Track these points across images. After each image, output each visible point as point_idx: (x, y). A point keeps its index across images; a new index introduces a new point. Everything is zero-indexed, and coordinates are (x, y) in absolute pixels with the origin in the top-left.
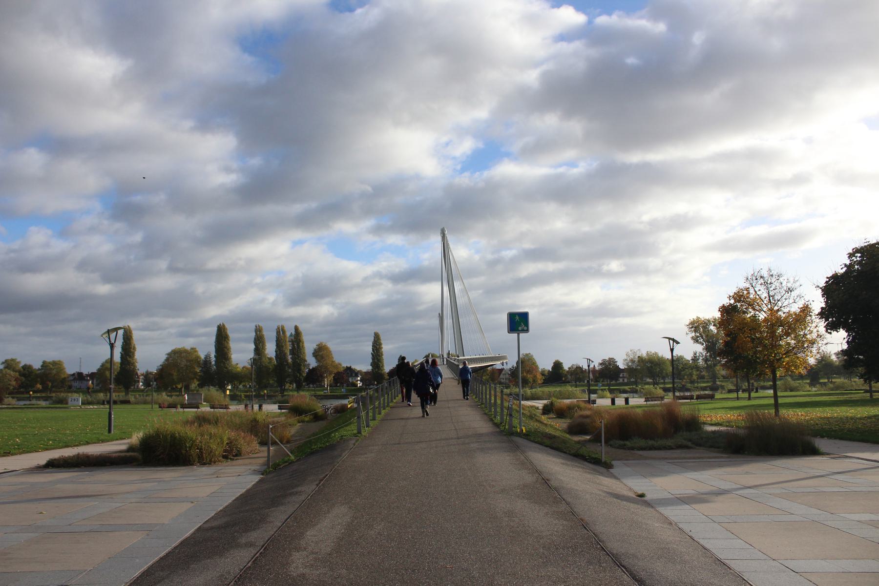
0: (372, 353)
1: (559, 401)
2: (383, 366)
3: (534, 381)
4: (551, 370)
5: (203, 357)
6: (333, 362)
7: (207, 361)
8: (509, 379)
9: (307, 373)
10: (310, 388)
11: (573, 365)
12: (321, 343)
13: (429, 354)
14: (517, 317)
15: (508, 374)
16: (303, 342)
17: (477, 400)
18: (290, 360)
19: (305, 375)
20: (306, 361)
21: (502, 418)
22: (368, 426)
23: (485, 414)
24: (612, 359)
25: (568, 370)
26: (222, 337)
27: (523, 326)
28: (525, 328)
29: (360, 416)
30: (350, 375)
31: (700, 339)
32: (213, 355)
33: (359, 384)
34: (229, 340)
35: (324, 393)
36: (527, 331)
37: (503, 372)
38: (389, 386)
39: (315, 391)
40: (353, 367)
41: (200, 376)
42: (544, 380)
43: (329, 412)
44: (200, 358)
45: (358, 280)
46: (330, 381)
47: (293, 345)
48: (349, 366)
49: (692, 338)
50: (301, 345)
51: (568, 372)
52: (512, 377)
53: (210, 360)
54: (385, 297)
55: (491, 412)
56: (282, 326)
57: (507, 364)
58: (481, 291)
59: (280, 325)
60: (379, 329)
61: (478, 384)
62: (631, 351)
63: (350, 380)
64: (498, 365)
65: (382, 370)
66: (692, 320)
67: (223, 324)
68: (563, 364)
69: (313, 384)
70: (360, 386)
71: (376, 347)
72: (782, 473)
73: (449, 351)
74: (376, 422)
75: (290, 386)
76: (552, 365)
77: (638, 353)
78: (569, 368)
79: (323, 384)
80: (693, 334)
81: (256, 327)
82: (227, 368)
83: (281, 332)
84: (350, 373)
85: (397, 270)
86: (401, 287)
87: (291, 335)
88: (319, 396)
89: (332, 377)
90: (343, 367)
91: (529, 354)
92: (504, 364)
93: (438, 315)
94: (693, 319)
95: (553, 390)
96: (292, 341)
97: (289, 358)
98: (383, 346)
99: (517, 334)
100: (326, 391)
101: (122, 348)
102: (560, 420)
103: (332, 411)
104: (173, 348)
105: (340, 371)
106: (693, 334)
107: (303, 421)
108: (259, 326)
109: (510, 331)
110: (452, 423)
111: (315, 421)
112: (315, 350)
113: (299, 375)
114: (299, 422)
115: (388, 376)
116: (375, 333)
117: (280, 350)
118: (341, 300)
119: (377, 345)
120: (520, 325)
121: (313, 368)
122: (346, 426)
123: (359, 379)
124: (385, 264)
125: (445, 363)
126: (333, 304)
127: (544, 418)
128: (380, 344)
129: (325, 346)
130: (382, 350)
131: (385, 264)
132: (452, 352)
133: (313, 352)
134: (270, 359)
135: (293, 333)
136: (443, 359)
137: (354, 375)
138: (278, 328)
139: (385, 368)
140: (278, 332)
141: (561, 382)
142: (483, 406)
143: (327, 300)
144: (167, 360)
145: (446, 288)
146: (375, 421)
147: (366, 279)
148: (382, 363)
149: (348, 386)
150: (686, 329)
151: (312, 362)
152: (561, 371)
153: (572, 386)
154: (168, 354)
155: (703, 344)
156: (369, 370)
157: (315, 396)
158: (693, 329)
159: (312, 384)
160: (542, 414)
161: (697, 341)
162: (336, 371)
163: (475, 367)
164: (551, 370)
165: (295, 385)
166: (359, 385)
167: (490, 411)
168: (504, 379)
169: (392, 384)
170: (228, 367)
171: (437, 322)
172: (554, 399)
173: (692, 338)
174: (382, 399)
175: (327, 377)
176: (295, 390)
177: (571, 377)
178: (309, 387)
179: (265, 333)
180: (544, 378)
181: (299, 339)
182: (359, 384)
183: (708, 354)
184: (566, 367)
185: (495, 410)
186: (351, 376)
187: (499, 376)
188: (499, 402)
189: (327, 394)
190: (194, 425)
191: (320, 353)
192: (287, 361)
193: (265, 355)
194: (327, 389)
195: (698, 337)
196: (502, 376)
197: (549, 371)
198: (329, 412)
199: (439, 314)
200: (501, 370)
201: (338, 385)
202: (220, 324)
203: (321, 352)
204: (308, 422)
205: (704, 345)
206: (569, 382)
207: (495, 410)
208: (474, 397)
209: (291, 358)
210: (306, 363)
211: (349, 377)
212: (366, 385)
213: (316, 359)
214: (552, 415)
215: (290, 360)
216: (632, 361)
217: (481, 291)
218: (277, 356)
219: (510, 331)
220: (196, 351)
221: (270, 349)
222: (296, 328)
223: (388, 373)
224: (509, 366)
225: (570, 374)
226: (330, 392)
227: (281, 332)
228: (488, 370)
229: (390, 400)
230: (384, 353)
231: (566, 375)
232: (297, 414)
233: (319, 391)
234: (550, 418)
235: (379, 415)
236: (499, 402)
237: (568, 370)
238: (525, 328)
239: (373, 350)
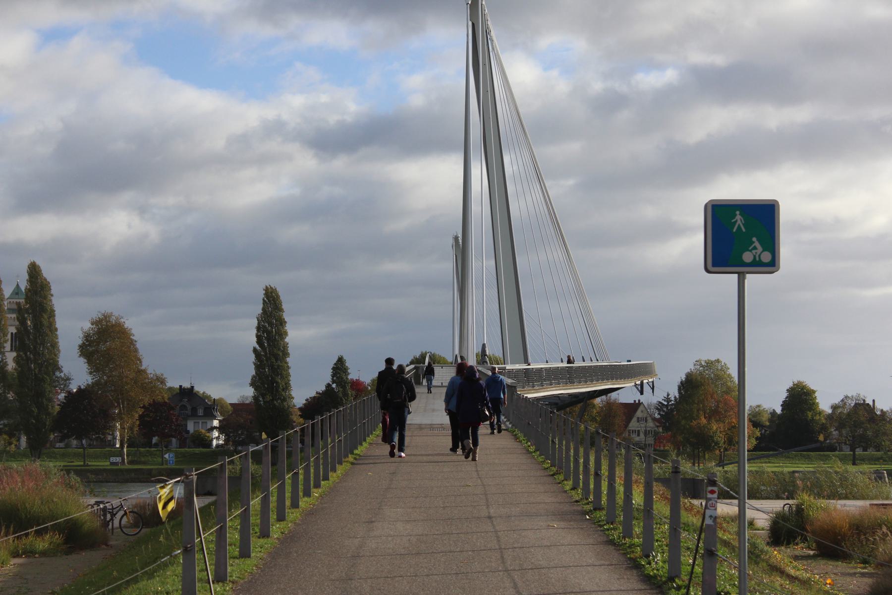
0: (255, 350)
1: (823, 503)
2: (287, 386)
3: (730, 441)
4: (779, 410)
8: (656, 434)
9: (64, 406)
10: (70, 450)
11: (846, 397)
12: (106, 317)
13: (426, 354)
14: (739, 218)
15: (654, 419)
17: (577, 495)
18: (11, 365)
19: (57, 408)
20: (60, 369)
21: (674, 561)
22: (220, 578)
23: (611, 542)
25: (830, 411)
27: (757, 250)
28: (766, 257)
29: (193, 546)
30: (189, 412)
33: (217, 439)
35: (112, 464)
36: (772, 265)
37: (639, 414)
39: (84, 457)
40: (200, 389)
42: (757, 439)
43: (116, 522)
45: (218, 143)
46: (131, 429)
47: (22, 321)
48: (186, 385)
51: (830, 417)
52: (666, 429)
54: (296, 191)
55: (631, 536)
57: (653, 389)
58: (571, 182)
60: (276, 281)
61: (581, 450)
63: (191, 427)
64: (626, 392)
65: (284, 400)
68: (816, 394)
69: (79, 438)
70: (218, 446)
71: (269, 333)
73: (484, 345)
74: (249, 565)
75: (10, 444)
76: (784, 395)
78: (835, 407)
79: (110, 438)
84: (189, 407)
85: (333, 119)
86: (340, 164)
87: (17, 292)
88: (98, 472)
89: (137, 416)
90: (170, 389)
91: (718, 361)
92: (647, 388)
93: (451, 241)
95: (786, 470)
96: (19, 310)
98: (288, 328)
99: (736, 276)
100: (119, 459)
102: (831, 566)
103: (125, 519)
105: (159, 399)
107: (29, 553)
109: (714, 265)
110: (506, 570)
111: (68, 552)
112: (87, 337)
113: (35, 410)
114: (16, 555)
115: (301, 416)
116: (266, 289)
118: (170, 200)
119: (271, 324)
120: (747, 246)
121: (80, 390)
122: (150, 575)
123: (216, 423)
124: (298, 101)
126: (142, 210)
127: (778, 555)
128: (282, 323)
130: (287, 340)
131: (298, 101)
132: (494, 350)
133: (80, 342)
135: (24, 285)
137: (201, 412)
139: (293, 393)
141: (813, 446)
142: (602, 515)
143: (127, 196)
145: (478, 171)
146: (248, 561)
147: (243, 140)
148: (286, 377)
149: (182, 444)
152: (810, 414)
153: (843, 459)
156: (247, 398)
157: (80, 472)
159: (76, 438)
160: (768, 544)
162: (147, 400)
164: (779, 410)
165: (24, 439)
166: (215, 442)
167: (628, 533)
168: (642, 436)
169: (308, 440)
171: (448, 267)
172: (806, 497)
174: (273, 488)
175: (120, 417)
176: (24, 455)
177: (841, 435)
178: (68, 446)
180: (758, 434)
182: (217, 439)
184: (825, 403)
185: (648, 533)
186: (194, 414)
187: (626, 426)
188: (638, 499)
189: (120, 467)
190: (618, 457)
191: (102, 347)
194: (121, 454)
196: (633, 425)
197: (773, 413)
198: (116, 522)
199: (456, 238)
200: (634, 407)
201: (155, 440)
204: (44, 554)
206: (832, 449)
207: (648, 533)
208: (569, 485)
209: (17, 360)
210: (58, 374)
211: (186, 418)
212: (236, 443)
213: (89, 362)
214: (800, 549)
215: (11, 365)
217: (571, 182)
219: (714, 265)
222: (34, 271)
223: (300, 409)
224: (658, 397)
225: (836, 424)
226: (130, 463)
228: (594, 406)
229: (301, 487)
230: (290, 350)
231: (824, 428)
232: (7, 527)
233: (96, 457)
234: (796, 558)
235: (262, 541)
236: (638, 499)
237: (830, 411)
238: (766, 257)
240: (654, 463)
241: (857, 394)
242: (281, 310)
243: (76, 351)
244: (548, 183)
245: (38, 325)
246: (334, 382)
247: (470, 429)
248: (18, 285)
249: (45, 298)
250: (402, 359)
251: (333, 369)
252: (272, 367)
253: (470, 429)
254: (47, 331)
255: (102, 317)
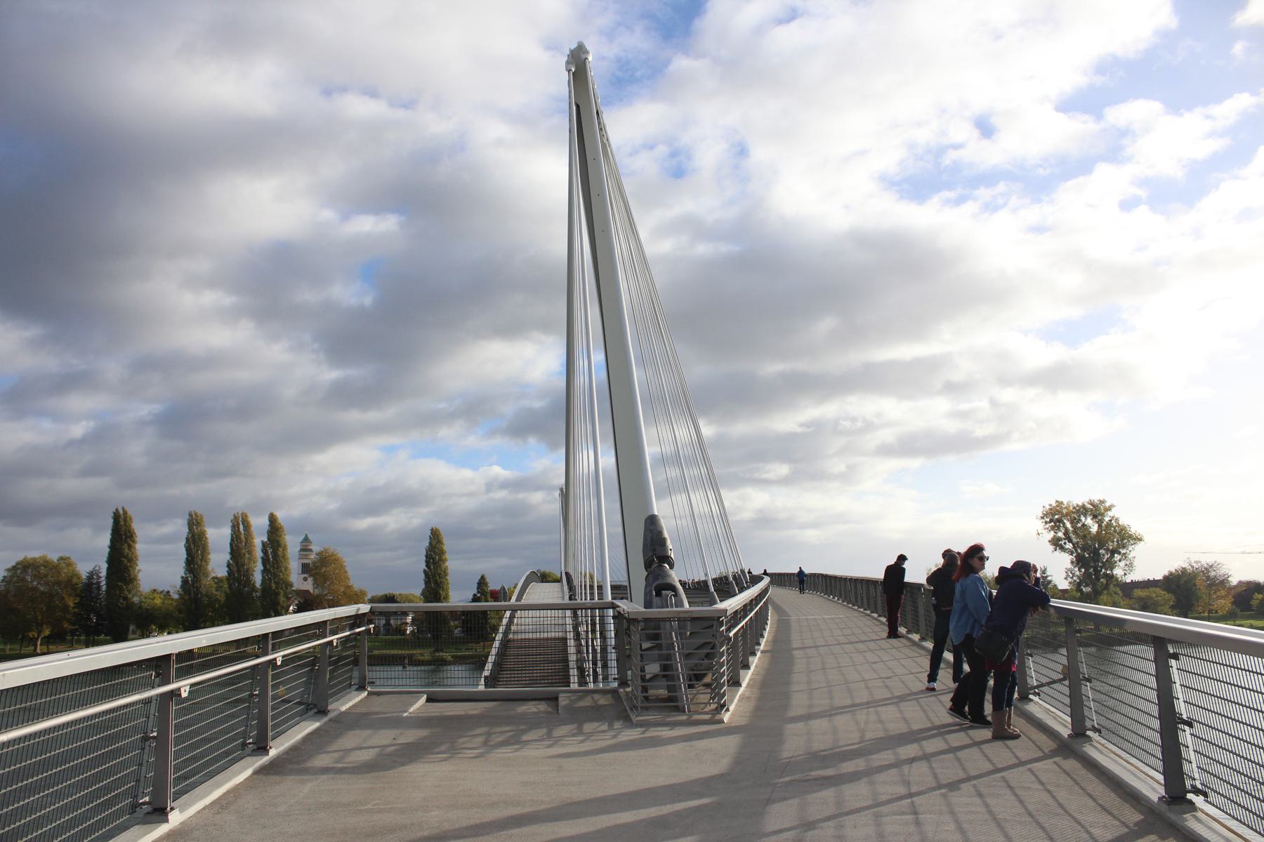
0: (425, 571)
5: (84, 575)
6: (348, 587)
7: (91, 584)
16: (286, 546)
26: (122, 534)
31: (1065, 543)
34: (134, 541)
38: (146, 812)
41: (75, 614)
44: (79, 577)
50: (280, 553)
56: (242, 515)
59: (240, 513)
60: (125, 498)
66: (1048, 507)
67: (123, 509)
72: (932, 677)
82: (126, 599)
83: (241, 527)
94: (1051, 505)
97: (257, 578)
104: (19, 557)
116: (432, 530)
117: (237, 563)
119: (434, 552)
128: (442, 552)
129: (333, 555)
138: (236, 518)
154: (8, 570)
161: (1062, 548)
163: (623, 308)
170: (130, 596)
181: (278, 542)
202: (238, 513)
220: (69, 565)
222: (273, 519)
227: (241, 527)
239: (428, 566)
240: (180, 695)
241: (1057, 501)
242: (442, 543)
244: (724, 493)
245: (275, 554)
246: (478, 592)
247: (1004, 659)
248: (306, 535)
249: (280, 536)
250: (115, 511)
251: (478, 583)
252: (436, 583)
253: (1004, 659)
254: (283, 560)
255: (323, 550)
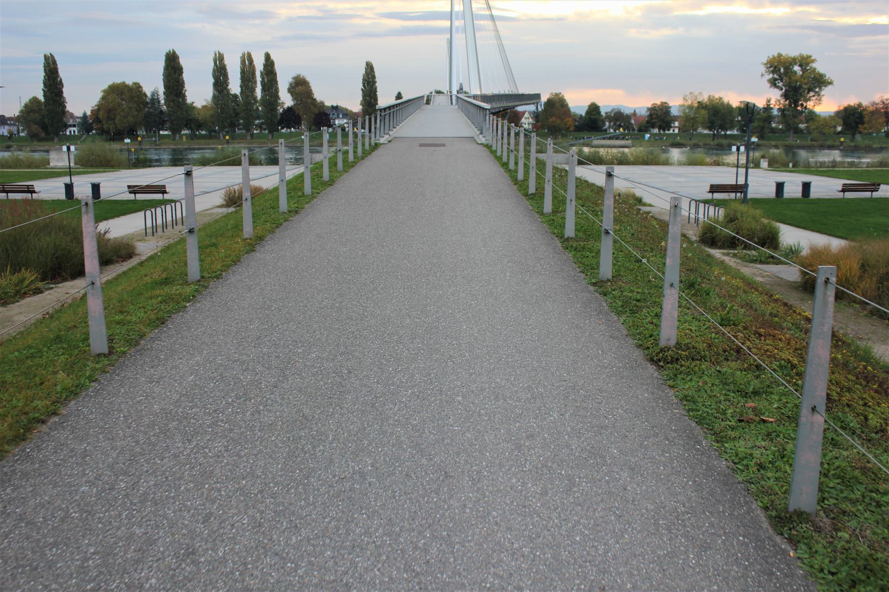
24: (665, 103)
32: (161, 90)
49: (769, 81)
53: (158, 99)
62: (690, 93)
77: (698, 97)
80: (771, 76)
81: (216, 55)
101: (44, 83)
106: (771, 76)
108: (219, 53)
125: (454, 102)
134: (235, 96)
136: (451, 96)
138: (244, 55)
140: (243, 62)
144: (103, 98)
150: (763, 69)
151: (286, 100)
155: (782, 89)
158: (771, 69)
173: (769, 81)
179: (227, 61)
183: (787, 102)
192: (255, 98)
193: (228, 93)
195: (776, 80)
197: (581, 116)
203: (300, 87)
205: (783, 91)
216: (690, 107)
218: (242, 92)
221: (235, 87)
222: (268, 57)
243: (286, 91)
